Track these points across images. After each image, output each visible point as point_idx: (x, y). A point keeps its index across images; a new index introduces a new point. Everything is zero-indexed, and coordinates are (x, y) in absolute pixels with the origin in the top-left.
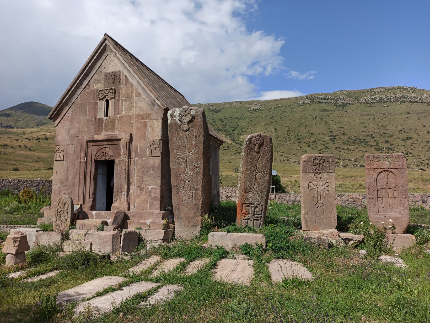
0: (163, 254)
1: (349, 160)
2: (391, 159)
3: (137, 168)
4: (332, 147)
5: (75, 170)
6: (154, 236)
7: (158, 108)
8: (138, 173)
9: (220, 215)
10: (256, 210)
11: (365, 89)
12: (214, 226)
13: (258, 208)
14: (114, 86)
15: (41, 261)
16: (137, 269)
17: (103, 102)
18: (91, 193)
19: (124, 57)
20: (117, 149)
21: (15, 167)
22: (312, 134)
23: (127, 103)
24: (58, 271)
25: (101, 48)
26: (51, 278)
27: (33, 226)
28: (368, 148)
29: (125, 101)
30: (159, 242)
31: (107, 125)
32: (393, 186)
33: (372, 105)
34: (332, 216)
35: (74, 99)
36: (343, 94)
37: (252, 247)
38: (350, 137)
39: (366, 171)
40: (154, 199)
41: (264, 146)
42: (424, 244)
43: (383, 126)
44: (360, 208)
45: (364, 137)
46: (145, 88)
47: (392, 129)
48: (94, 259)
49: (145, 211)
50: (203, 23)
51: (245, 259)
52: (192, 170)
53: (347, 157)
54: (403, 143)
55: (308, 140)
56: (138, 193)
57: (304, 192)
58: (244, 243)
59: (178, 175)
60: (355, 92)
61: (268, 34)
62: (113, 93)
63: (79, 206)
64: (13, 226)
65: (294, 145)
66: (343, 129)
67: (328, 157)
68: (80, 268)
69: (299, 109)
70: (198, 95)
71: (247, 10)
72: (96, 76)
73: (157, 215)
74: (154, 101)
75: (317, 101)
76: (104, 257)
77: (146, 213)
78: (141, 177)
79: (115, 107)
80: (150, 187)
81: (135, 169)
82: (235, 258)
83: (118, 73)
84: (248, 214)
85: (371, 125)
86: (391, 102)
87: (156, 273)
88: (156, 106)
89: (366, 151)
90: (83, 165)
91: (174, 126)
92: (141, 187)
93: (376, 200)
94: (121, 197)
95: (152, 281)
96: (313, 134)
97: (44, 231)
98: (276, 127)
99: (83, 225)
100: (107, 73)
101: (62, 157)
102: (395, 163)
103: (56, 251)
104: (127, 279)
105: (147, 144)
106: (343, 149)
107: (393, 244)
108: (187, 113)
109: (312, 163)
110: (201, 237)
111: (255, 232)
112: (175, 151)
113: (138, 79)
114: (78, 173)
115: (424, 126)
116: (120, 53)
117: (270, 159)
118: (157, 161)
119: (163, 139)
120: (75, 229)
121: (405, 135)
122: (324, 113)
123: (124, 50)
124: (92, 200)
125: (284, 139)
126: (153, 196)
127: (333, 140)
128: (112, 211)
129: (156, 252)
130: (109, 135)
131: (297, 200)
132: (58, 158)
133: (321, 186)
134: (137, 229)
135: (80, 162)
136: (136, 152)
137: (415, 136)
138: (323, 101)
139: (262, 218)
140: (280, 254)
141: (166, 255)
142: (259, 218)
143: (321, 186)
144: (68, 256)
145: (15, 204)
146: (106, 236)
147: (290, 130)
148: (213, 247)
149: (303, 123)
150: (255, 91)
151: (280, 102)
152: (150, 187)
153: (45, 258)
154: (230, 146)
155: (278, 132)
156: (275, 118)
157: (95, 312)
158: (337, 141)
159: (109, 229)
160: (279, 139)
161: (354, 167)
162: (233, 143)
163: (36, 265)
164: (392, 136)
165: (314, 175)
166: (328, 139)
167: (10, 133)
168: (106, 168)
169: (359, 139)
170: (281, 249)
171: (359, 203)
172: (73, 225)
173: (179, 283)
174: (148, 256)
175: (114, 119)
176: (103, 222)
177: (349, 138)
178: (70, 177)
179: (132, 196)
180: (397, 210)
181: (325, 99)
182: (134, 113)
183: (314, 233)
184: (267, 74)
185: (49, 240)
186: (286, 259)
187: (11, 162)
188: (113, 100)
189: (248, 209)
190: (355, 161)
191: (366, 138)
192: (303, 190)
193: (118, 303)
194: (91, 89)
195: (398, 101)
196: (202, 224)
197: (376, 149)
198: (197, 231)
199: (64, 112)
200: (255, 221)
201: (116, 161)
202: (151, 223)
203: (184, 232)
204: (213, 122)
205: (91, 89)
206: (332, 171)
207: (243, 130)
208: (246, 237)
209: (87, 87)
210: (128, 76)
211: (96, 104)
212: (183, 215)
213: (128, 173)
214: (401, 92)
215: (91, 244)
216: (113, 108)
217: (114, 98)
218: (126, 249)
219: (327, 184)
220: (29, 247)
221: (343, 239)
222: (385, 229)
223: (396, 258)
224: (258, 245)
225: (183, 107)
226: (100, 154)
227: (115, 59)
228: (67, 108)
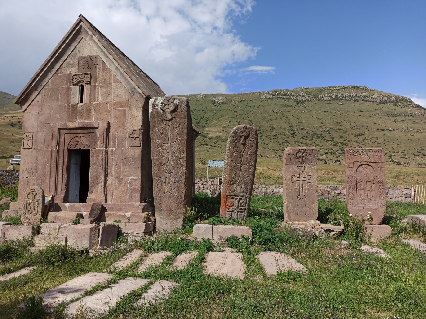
0: (147, 248)
2: (370, 153)
3: (115, 158)
5: (46, 159)
6: (134, 229)
7: (139, 95)
8: (117, 163)
9: (205, 208)
11: (323, 87)
12: (196, 219)
13: (242, 201)
14: (89, 71)
16: (122, 264)
17: (78, 88)
19: (101, 40)
20: (93, 138)
22: (273, 128)
23: (104, 90)
24: (31, 268)
25: (76, 30)
26: (24, 276)
28: (324, 143)
29: (101, 87)
30: (140, 235)
31: (81, 111)
32: (371, 179)
33: (329, 103)
34: (314, 208)
35: (44, 83)
36: (303, 91)
37: (238, 239)
38: (308, 132)
39: (346, 164)
40: (134, 190)
41: (250, 138)
42: (399, 234)
43: (338, 123)
44: (328, 200)
45: (321, 133)
46: (125, 74)
47: (346, 126)
48: (71, 254)
49: (124, 203)
51: (232, 252)
52: (175, 161)
54: (356, 139)
55: (269, 134)
56: (117, 184)
57: (287, 184)
58: (230, 235)
60: (314, 90)
62: (89, 79)
63: (50, 198)
68: (56, 264)
69: (262, 104)
70: (175, 86)
72: (70, 60)
73: (138, 207)
74: (135, 88)
75: (279, 96)
76: (82, 252)
78: (119, 168)
79: (90, 93)
80: (130, 179)
81: (112, 159)
82: (222, 251)
83: (94, 57)
85: (327, 121)
86: (346, 100)
87: (143, 269)
88: (136, 94)
90: (54, 154)
91: (156, 116)
92: (119, 179)
93: (356, 192)
94: (98, 188)
95: (141, 277)
96: (274, 128)
97: (11, 224)
98: (239, 120)
99: (56, 218)
100: (82, 57)
102: (374, 157)
103: (27, 246)
104: (114, 276)
105: (127, 133)
106: (302, 143)
108: (170, 102)
109: (295, 156)
110: (183, 229)
111: (241, 224)
112: (157, 141)
113: (117, 64)
114: (49, 162)
115: (375, 124)
116: (97, 36)
117: (255, 151)
118: (137, 152)
119: (143, 128)
120: (47, 222)
121: (357, 132)
124: (65, 191)
126: (132, 188)
127: (293, 134)
128: (87, 203)
129: (138, 245)
130: (84, 122)
131: (268, 191)
132: (26, 146)
133: (303, 179)
134: (116, 221)
135: (52, 151)
137: (367, 132)
138: (284, 97)
139: (246, 210)
140: (267, 246)
141: (149, 249)
142: (243, 210)
143: (303, 179)
144: (42, 252)
146: (83, 230)
147: (252, 124)
148: (198, 240)
149: (265, 117)
151: (244, 96)
152: (130, 179)
153: (14, 254)
156: (238, 112)
157: (89, 313)
159: (85, 223)
163: (4, 262)
164: (346, 131)
170: (270, 241)
171: (327, 195)
173: (171, 279)
174: (130, 250)
176: (78, 215)
177: (308, 133)
178: (40, 167)
179: (110, 188)
181: (286, 95)
182: (112, 101)
183: (297, 224)
185: (18, 235)
186: (273, 250)
188: (89, 86)
189: (232, 202)
191: (322, 133)
192: (286, 182)
193: (113, 303)
194: (64, 73)
195: (352, 100)
196: (185, 216)
197: (331, 144)
198: (180, 223)
199: (33, 96)
200: (239, 213)
201: (92, 150)
202: (131, 215)
203: (166, 224)
206: (314, 164)
207: (208, 122)
208: (232, 229)
209: (59, 70)
210: (105, 61)
211: (69, 89)
212: (164, 207)
213: (105, 163)
215: (66, 238)
216: (89, 94)
217: (90, 84)
218: (105, 243)
221: (324, 230)
222: (364, 220)
223: (376, 248)
224: (244, 238)
226: (73, 142)
227: (91, 42)
228: (37, 92)
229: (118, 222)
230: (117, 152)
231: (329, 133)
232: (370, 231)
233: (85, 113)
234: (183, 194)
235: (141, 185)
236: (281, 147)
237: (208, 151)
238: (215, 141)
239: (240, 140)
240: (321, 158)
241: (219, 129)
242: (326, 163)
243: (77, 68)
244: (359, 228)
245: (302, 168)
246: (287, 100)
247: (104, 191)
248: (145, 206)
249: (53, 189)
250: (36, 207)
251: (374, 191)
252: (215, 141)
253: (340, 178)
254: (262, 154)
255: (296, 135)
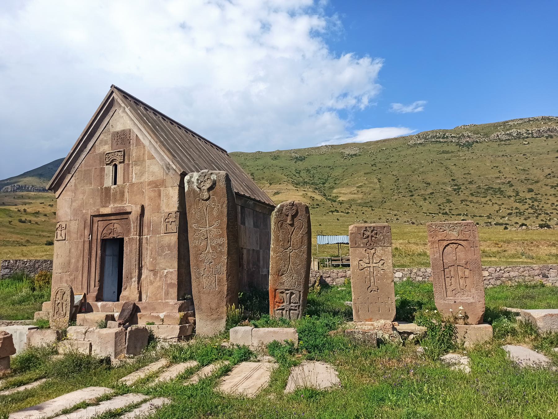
1: (480, 216)
2: (459, 228)
3: (150, 248)
4: (456, 199)
6: (167, 332)
10: (292, 297)
12: (245, 319)
15: (29, 367)
17: (111, 167)
18: (97, 280)
21: (49, 239)
22: (427, 184)
25: (108, 103)
27: (28, 321)
29: (135, 165)
31: (115, 194)
34: (390, 302)
35: (77, 165)
38: (479, 186)
40: (170, 285)
41: (299, 217)
43: (524, 170)
46: (159, 149)
47: (536, 173)
49: (160, 301)
50: (273, 48)
51: (269, 362)
52: (213, 248)
53: (477, 212)
56: (152, 278)
59: (197, 255)
60: (484, 127)
61: (361, 57)
63: (81, 297)
64: (9, 321)
65: (405, 198)
66: (469, 176)
67: (381, 227)
69: (409, 152)
71: (327, 28)
73: (173, 306)
74: (169, 164)
75: (433, 140)
76: (102, 361)
77: (159, 303)
79: (124, 173)
80: (166, 271)
81: (147, 249)
82: (259, 361)
84: (282, 303)
85: (507, 169)
86: (533, 137)
88: (171, 171)
89: (503, 204)
90: (87, 245)
91: (192, 195)
92: (154, 272)
93: (443, 280)
94: (132, 283)
96: (429, 184)
97: (38, 328)
98: (379, 176)
99: (85, 320)
101: (63, 235)
102: (464, 234)
106: (471, 202)
107: (465, 338)
108: (206, 178)
113: (150, 138)
114: (82, 255)
117: (307, 233)
118: (173, 239)
122: (443, 155)
123: (137, 102)
125: (391, 192)
126: (168, 282)
127: (457, 190)
130: (117, 207)
133: (374, 265)
136: (149, 227)
138: (441, 140)
142: (296, 307)
143: (374, 265)
145: (25, 291)
146: (108, 335)
147: (398, 179)
149: (415, 170)
150: (347, 129)
151: (384, 143)
152: (166, 271)
154: (320, 203)
155: (383, 183)
156: (378, 165)
158: (462, 191)
160: (384, 192)
161: (487, 225)
162: (324, 200)
163: (23, 372)
164: (537, 182)
165: (366, 251)
166: (450, 189)
167: (43, 198)
168: (113, 247)
169: (492, 188)
170: (315, 347)
172: (73, 320)
175: (123, 188)
178: (73, 261)
180: (469, 293)
181: (443, 138)
184: (362, 107)
187: (45, 234)
188: (122, 164)
190: (489, 217)
191: (501, 186)
194: (97, 152)
195: (543, 136)
196: (228, 317)
197: (515, 201)
199: (66, 180)
200: (291, 311)
201: (126, 239)
203: (204, 327)
204: (297, 173)
205: (97, 152)
206: (388, 245)
207: (337, 182)
208: (274, 332)
211: (102, 170)
212: (204, 306)
213: (139, 254)
214: (546, 123)
215: (91, 344)
216: (122, 175)
217: (123, 162)
218: (132, 350)
219: (382, 262)
220: (15, 350)
221: (400, 333)
222: (456, 318)
225: (202, 171)
226: (107, 231)
227: (124, 115)
229: (151, 324)
230: (152, 240)
231: (512, 186)
232: (463, 333)
233: (118, 196)
234: (226, 288)
235: (178, 279)
236: (440, 209)
237: (338, 220)
238: (347, 206)
239: (287, 219)
240: (501, 221)
241: (352, 189)
242: (506, 228)
243: (110, 145)
244: (451, 330)
245: (373, 251)
246: (445, 145)
247: (138, 287)
248: (182, 304)
249: (85, 286)
250: (64, 308)
251: (468, 279)
252: (347, 206)
253: (513, 252)
254: (414, 221)
255: (462, 191)
